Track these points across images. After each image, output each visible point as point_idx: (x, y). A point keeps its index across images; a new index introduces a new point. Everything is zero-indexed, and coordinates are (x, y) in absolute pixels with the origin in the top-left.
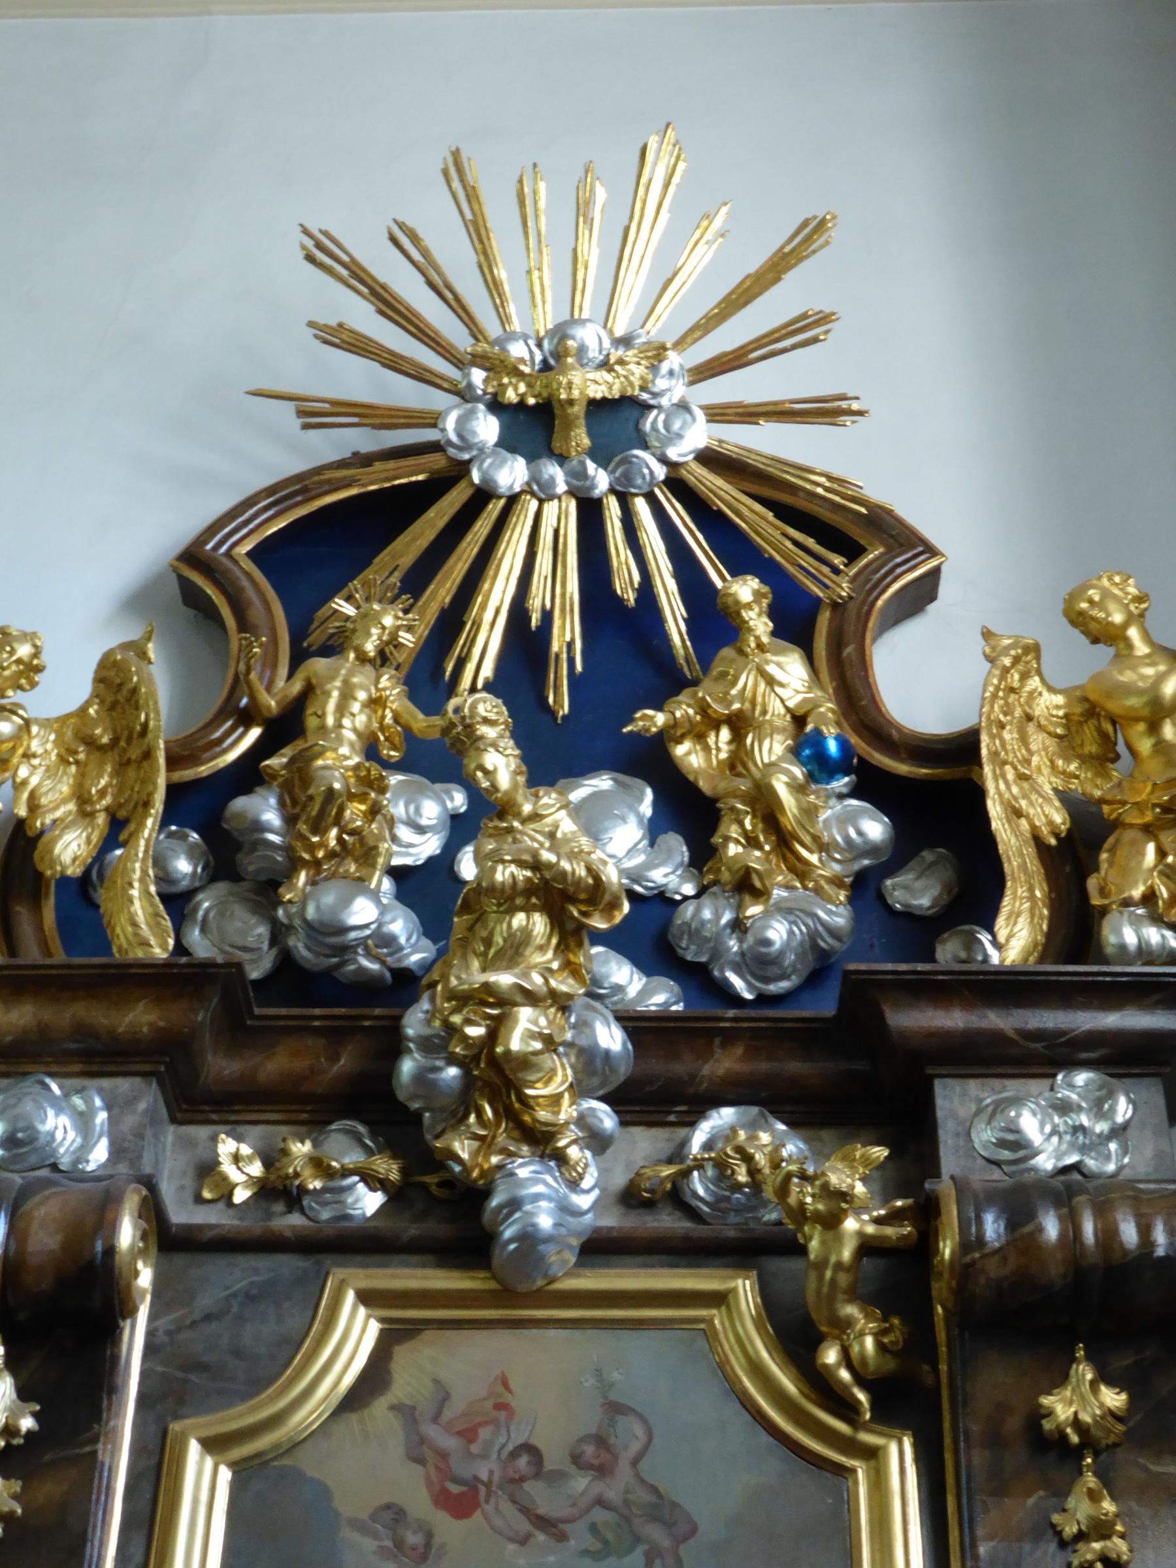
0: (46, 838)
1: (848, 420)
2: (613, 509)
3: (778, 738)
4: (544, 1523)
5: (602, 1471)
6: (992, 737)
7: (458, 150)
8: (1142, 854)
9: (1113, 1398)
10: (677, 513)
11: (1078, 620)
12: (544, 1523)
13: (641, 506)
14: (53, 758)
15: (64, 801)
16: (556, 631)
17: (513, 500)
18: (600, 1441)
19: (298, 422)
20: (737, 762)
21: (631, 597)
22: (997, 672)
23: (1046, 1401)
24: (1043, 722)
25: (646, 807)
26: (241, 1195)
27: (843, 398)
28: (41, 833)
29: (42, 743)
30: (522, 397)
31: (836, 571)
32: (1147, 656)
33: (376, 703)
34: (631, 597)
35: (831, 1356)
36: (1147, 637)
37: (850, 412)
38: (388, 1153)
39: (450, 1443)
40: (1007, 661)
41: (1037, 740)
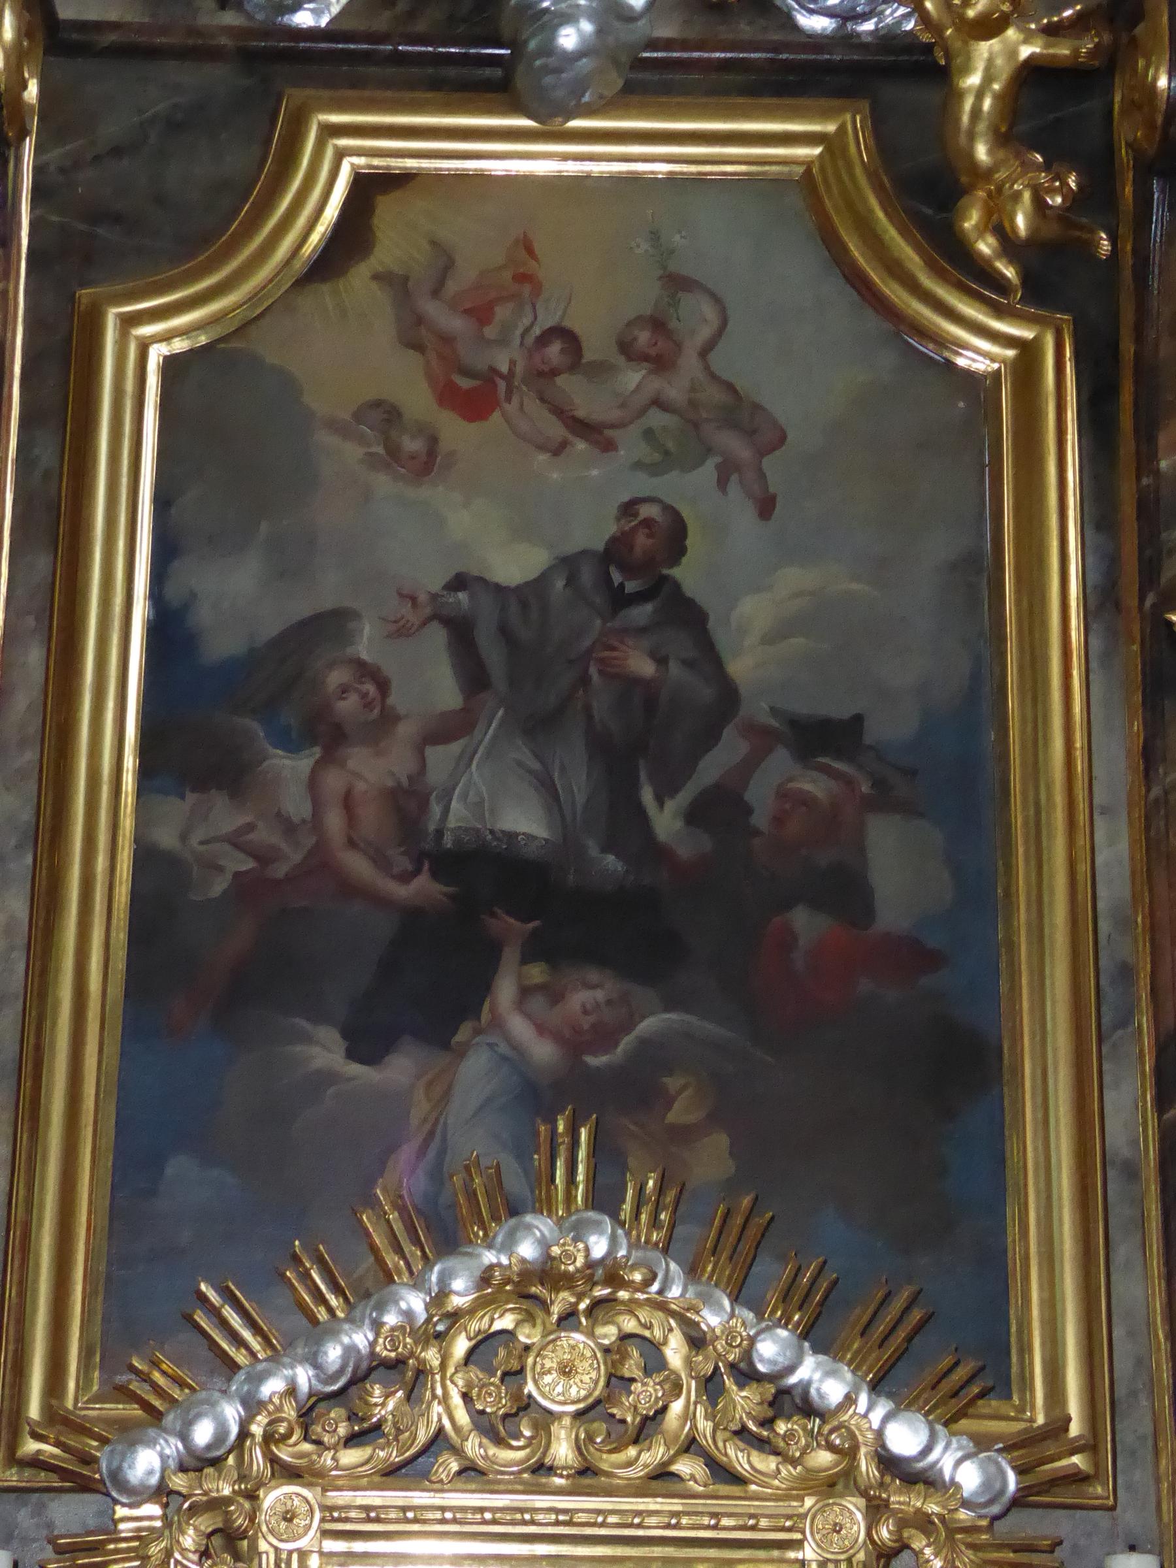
5: (661, 363)
18: (658, 324)
35: (971, 221)
39: (456, 324)
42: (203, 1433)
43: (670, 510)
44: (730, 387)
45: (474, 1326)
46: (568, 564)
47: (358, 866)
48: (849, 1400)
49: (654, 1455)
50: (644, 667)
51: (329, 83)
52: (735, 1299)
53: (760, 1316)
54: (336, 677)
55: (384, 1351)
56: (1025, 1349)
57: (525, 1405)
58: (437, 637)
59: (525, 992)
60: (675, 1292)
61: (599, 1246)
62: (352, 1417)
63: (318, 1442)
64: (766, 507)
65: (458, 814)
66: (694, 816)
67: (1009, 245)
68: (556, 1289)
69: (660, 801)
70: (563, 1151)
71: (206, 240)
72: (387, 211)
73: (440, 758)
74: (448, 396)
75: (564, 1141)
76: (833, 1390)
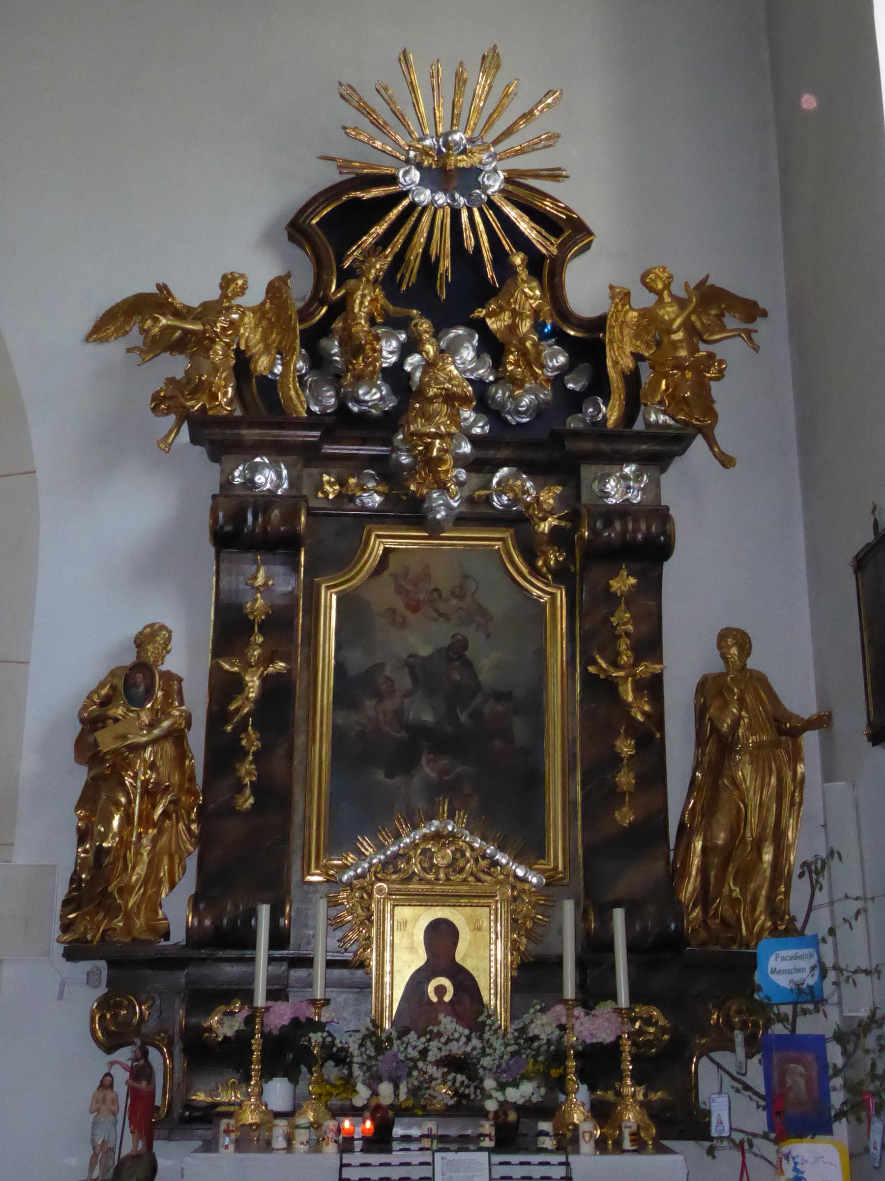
0: (253, 359)
1: (561, 179)
2: (464, 215)
3: (528, 320)
4: (441, 615)
5: (461, 597)
6: (610, 332)
7: (405, 49)
8: (661, 384)
9: (632, 581)
10: (490, 214)
11: (645, 284)
12: (441, 615)
13: (475, 210)
14: (253, 324)
15: (259, 343)
16: (441, 264)
17: (425, 208)
18: (461, 587)
19: (337, 171)
20: (512, 328)
21: (471, 250)
22: (613, 305)
23: (611, 582)
24: (629, 323)
25: (475, 342)
26: (331, 497)
27: (559, 169)
28: (251, 357)
29: (249, 319)
30: (431, 165)
31: (552, 243)
32: (670, 303)
33: (374, 300)
34: (471, 250)
35: (540, 563)
36: (671, 295)
37: (560, 176)
38: (384, 483)
39: (410, 587)
40: (617, 300)
41: (626, 331)
42: (359, 871)
43: (463, 637)
44: (479, 604)
45: (422, 847)
46: (439, 651)
47: (387, 728)
48: (508, 863)
49: (464, 876)
50: (457, 677)
51: (376, 523)
52: (482, 839)
53: (487, 843)
54: (381, 681)
55: (401, 852)
56: (549, 848)
57: (433, 865)
58: (406, 670)
59: (428, 761)
60: (468, 839)
61: (450, 828)
62: (394, 867)
63: (387, 873)
64: (488, 635)
65: (411, 716)
66: (470, 716)
67: (549, 570)
68: (441, 838)
69: (462, 713)
70: (442, 805)
71: (348, 564)
72: (391, 556)
73: (407, 701)
74: (408, 606)
75: (442, 803)
76: (504, 861)
